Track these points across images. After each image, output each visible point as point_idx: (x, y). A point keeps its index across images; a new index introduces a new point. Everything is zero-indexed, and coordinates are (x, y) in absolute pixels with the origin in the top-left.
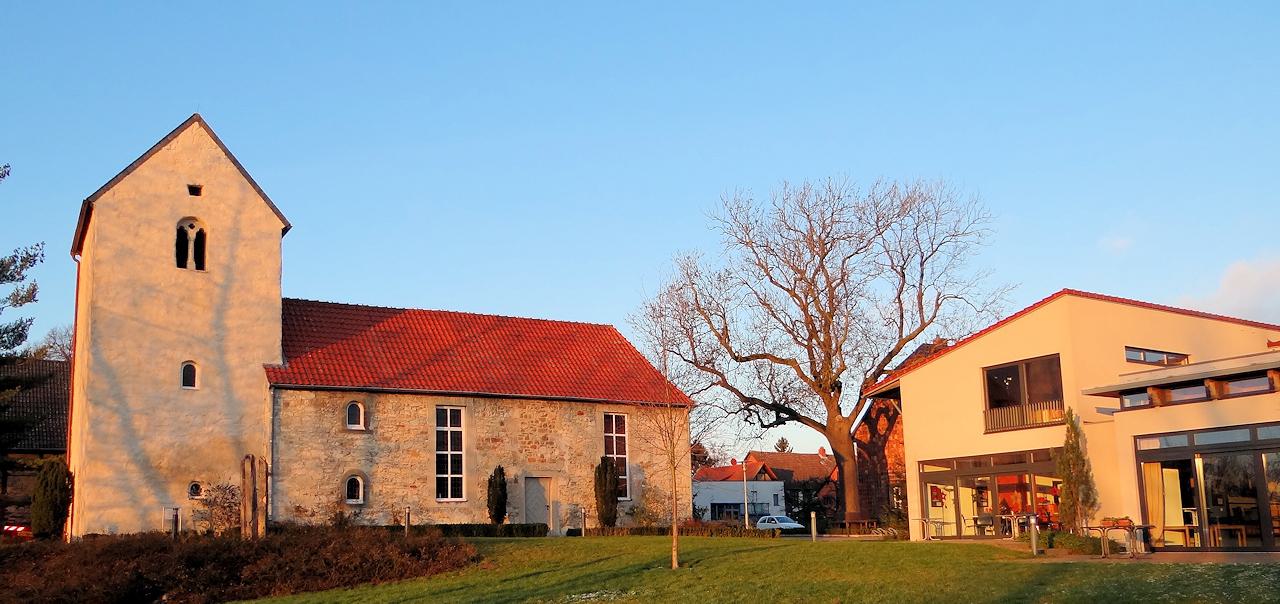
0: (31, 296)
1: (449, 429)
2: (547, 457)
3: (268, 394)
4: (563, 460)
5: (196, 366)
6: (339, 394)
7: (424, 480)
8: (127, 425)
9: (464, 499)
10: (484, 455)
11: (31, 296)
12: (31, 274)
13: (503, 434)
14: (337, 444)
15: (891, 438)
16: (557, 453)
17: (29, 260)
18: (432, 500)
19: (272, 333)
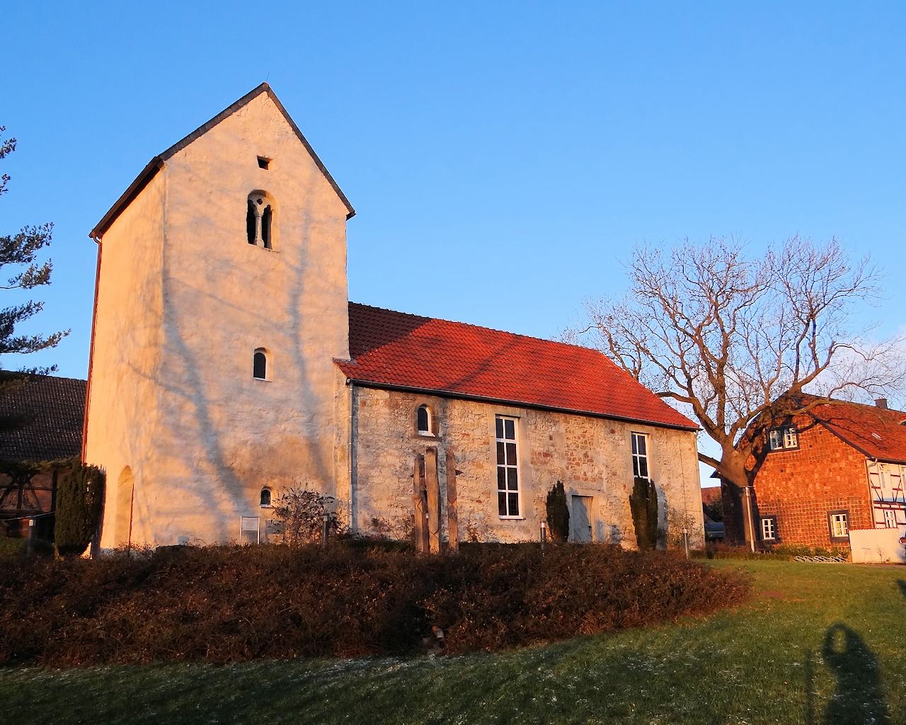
0: (44, 278)
1: (504, 441)
2: (589, 475)
3: (346, 392)
4: (601, 478)
5: (266, 355)
6: (411, 396)
7: (487, 494)
8: (202, 414)
9: (520, 516)
10: (537, 470)
11: (44, 278)
12: (40, 257)
13: (552, 449)
14: (410, 451)
15: (759, 474)
16: (596, 471)
17: (36, 241)
18: (496, 517)
19: (340, 326)
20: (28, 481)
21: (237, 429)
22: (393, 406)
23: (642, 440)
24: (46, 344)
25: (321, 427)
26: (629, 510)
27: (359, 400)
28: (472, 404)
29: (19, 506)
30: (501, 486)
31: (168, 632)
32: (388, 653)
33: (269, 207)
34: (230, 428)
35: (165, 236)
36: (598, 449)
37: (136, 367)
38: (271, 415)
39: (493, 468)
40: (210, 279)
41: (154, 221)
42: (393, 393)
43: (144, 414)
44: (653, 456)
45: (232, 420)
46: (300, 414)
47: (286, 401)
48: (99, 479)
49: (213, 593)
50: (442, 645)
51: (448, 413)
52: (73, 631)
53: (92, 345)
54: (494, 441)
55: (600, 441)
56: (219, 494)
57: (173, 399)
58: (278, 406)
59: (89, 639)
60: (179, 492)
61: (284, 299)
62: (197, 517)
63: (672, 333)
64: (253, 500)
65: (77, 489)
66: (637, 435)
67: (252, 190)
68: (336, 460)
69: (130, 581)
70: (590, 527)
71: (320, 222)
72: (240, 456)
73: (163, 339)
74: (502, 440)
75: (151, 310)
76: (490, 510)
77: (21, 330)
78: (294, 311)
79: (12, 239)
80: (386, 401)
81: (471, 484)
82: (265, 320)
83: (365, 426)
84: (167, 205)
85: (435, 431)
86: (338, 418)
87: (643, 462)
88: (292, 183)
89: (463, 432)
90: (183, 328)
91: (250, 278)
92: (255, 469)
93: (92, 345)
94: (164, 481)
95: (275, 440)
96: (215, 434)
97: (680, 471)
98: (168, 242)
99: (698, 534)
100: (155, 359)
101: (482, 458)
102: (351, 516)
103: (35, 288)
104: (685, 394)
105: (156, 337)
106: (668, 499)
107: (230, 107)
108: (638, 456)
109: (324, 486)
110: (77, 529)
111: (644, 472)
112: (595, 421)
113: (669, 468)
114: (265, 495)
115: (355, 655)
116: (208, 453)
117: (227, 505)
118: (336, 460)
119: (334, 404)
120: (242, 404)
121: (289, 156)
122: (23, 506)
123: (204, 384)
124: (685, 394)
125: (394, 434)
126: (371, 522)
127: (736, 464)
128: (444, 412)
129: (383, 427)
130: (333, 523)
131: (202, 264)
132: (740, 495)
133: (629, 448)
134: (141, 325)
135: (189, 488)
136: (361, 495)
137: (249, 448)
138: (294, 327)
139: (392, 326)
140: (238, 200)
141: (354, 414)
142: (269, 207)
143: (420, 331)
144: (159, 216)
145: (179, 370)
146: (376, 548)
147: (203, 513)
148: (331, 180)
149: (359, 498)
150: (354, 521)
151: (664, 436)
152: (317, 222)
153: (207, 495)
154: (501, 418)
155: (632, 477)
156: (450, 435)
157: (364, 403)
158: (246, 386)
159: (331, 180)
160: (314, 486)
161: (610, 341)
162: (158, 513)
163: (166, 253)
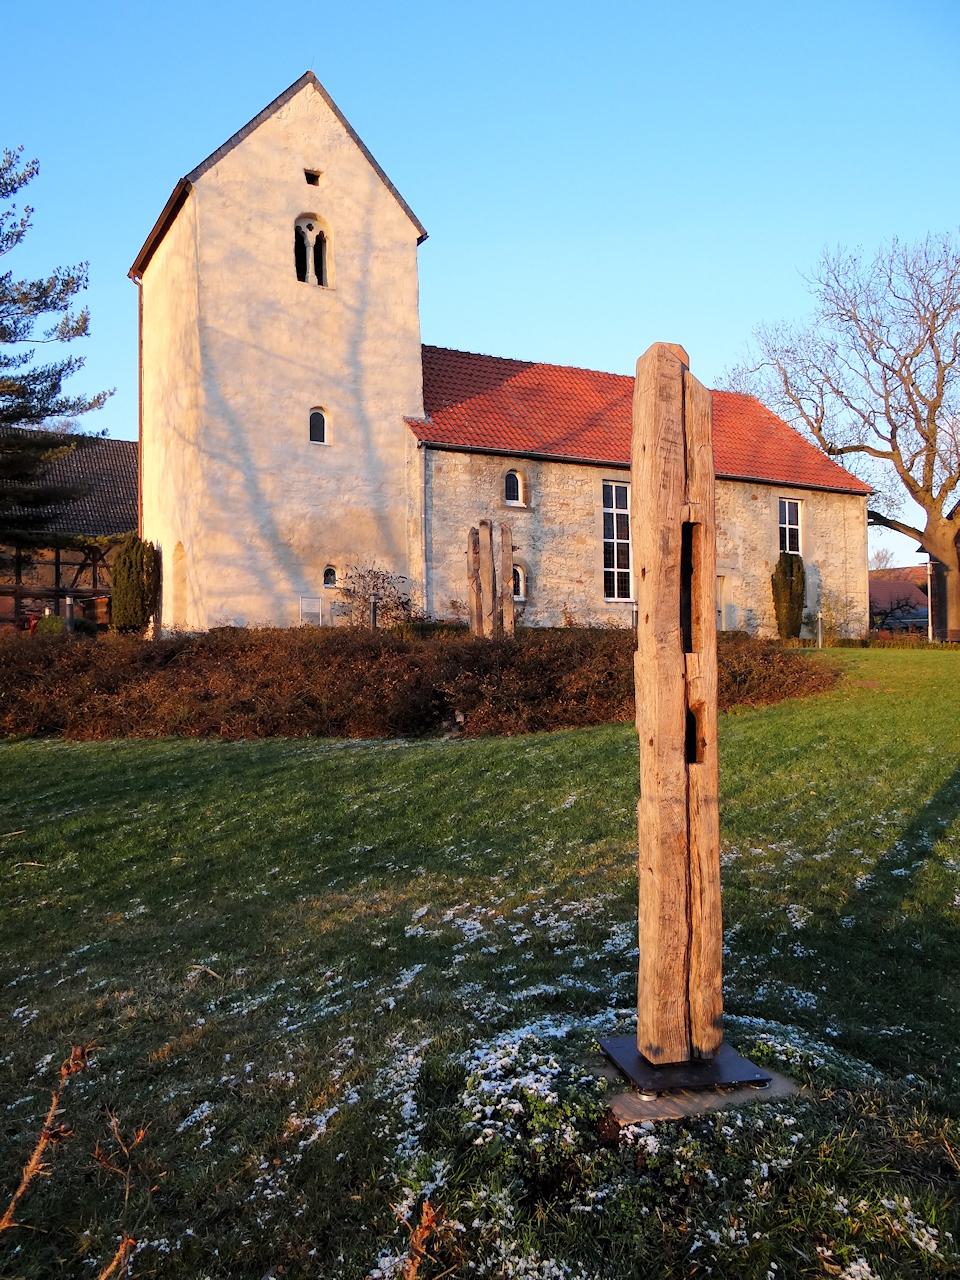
1: (614, 511)
3: (418, 456)
4: (736, 554)
6: (497, 459)
8: (252, 484)
11: (82, 328)
12: (77, 302)
16: (730, 546)
17: (71, 285)
19: (412, 376)
20: (101, 558)
21: (293, 501)
22: (475, 472)
23: (794, 508)
24: (91, 406)
25: (392, 497)
26: (769, 592)
27: (433, 465)
28: (573, 468)
29: (95, 586)
30: (608, 563)
31: (183, 711)
32: (402, 734)
33: (322, 233)
34: (285, 500)
35: (199, 277)
36: (734, 520)
37: (181, 431)
38: (332, 485)
39: (598, 544)
40: (253, 326)
41: (188, 258)
42: (475, 456)
43: (191, 485)
44: (807, 526)
45: (286, 492)
46: (367, 483)
47: (350, 467)
48: (156, 556)
49: (237, 673)
50: (461, 729)
51: (544, 479)
52: (94, 707)
53: (141, 405)
54: (600, 510)
55: (737, 509)
56: (276, 573)
57: (219, 468)
58: (338, 475)
59: (109, 714)
60: (231, 571)
61: (342, 347)
62: (253, 597)
63: (874, 367)
64: (315, 580)
65: (131, 566)
66: (787, 501)
67: (299, 213)
68: (409, 536)
69: (158, 661)
70: (720, 612)
71: (383, 249)
72: (298, 530)
73: (202, 400)
74: (611, 511)
75: (190, 366)
76: (593, 591)
77: (69, 389)
78: (353, 360)
79: (45, 283)
80: (466, 466)
81: (569, 563)
82: (321, 374)
83: (440, 496)
84: (199, 238)
85: (527, 500)
86: (409, 487)
87: (794, 534)
88: (347, 202)
89: (562, 501)
90: (226, 385)
91: (300, 324)
92: (316, 545)
93: (141, 405)
94: (215, 559)
95: (337, 512)
96: (269, 507)
97: (842, 544)
98: (203, 283)
99: (859, 620)
100: (196, 423)
101: (584, 531)
102: (425, 598)
103: (73, 340)
104: (887, 447)
105: (197, 396)
106: (823, 578)
107: (267, 107)
108: (787, 526)
109: (396, 564)
110: (134, 609)
111: (794, 546)
112: (731, 485)
113: (827, 541)
114: (329, 575)
115: (365, 736)
116: (262, 527)
117: (284, 586)
118: (409, 536)
119: (406, 471)
120: (297, 472)
121: (343, 169)
122: (99, 586)
123: (253, 451)
124: (887, 447)
125: (475, 506)
126: (449, 605)
127: (944, 534)
128: (538, 477)
129: (463, 497)
130: (405, 605)
131: (243, 308)
132: (945, 573)
133: (776, 516)
134: (182, 383)
135: (243, 566)
136: (436, 574)
137: (308, 522)
138: (355, 381)
139: (482, 374)
140: (282, 228)
141: (426, 482)
142: (322, 233)
143: (521, 380)
144: (191, 253)
145: (224, 435)
146: (445, 632)
147: (259, 594)
148: (396, 194)
149: (435, 577)
150: (429, 602)
151: (824, 502)
152: (380, 250)
153: (262, 574)
154: (610, 483)
155: (777, 552)
156: (544, 505)
157: (439, 469)
158: (300, 451)
159: (396, 194)
160: (383, 565)
161: (786, 382)
162: (210, 593)
163: (202, 297)
